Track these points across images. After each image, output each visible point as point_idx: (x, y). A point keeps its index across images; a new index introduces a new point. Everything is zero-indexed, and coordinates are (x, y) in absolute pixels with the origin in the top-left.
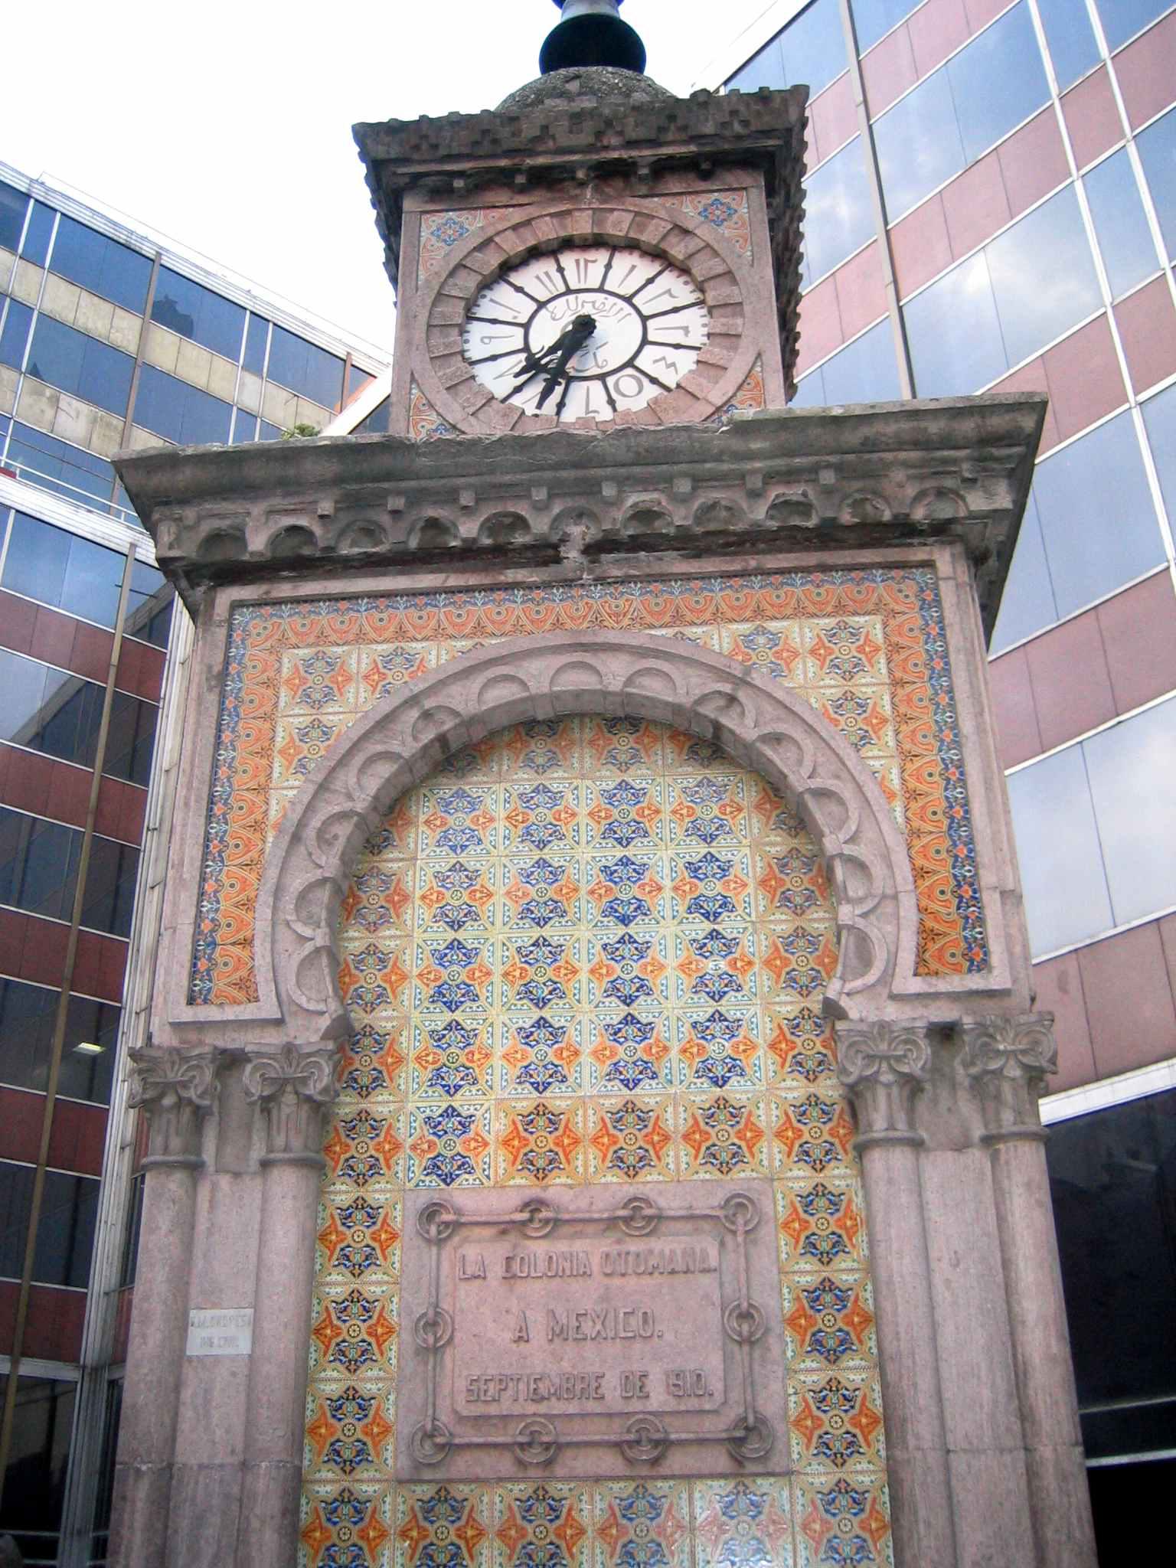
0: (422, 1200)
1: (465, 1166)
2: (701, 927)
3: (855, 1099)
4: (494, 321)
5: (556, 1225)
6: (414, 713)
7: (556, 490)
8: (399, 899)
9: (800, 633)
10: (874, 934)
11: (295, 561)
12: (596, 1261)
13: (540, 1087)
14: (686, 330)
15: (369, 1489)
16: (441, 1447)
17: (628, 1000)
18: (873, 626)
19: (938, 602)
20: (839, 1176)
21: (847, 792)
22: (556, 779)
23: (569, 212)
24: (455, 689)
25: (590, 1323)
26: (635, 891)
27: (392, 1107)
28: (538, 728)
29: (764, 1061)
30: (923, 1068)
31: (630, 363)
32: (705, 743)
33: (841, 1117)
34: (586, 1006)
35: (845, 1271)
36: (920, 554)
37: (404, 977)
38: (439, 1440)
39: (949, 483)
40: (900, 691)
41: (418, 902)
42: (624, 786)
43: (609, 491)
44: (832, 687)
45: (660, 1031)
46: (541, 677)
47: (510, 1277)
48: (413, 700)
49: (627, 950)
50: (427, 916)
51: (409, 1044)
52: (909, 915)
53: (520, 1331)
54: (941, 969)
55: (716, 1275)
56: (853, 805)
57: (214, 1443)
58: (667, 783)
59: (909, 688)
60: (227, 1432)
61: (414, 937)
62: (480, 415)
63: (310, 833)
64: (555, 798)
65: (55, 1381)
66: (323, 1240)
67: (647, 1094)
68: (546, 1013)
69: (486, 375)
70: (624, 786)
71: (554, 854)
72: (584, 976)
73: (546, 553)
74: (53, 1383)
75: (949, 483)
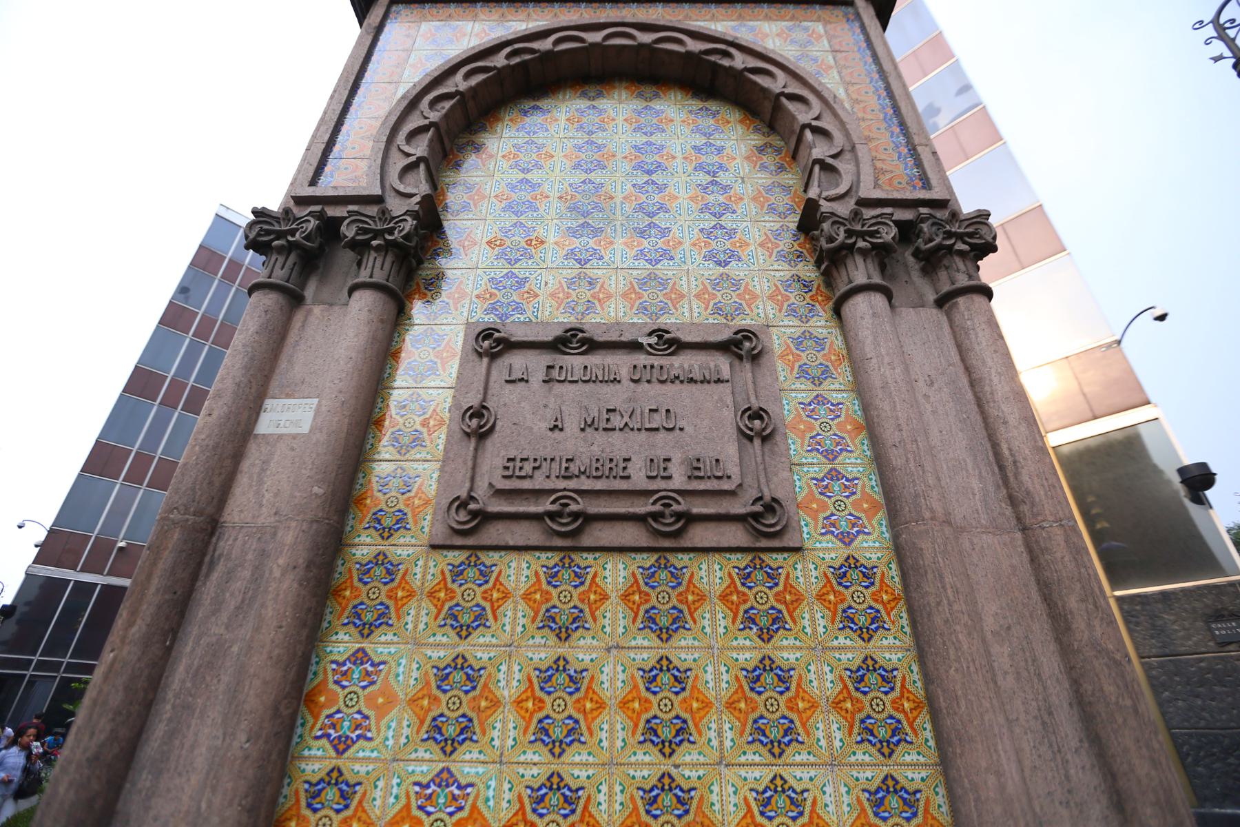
12: (624, 373)
15: (403, 552)
16: (474, 514)
25: (619, 418)
30: (893, 238)
33: (818, 288)
38: (472, 506)
53: (556, 420)
55: (729, 384)
57: (261, 506)
60: (276, 495)
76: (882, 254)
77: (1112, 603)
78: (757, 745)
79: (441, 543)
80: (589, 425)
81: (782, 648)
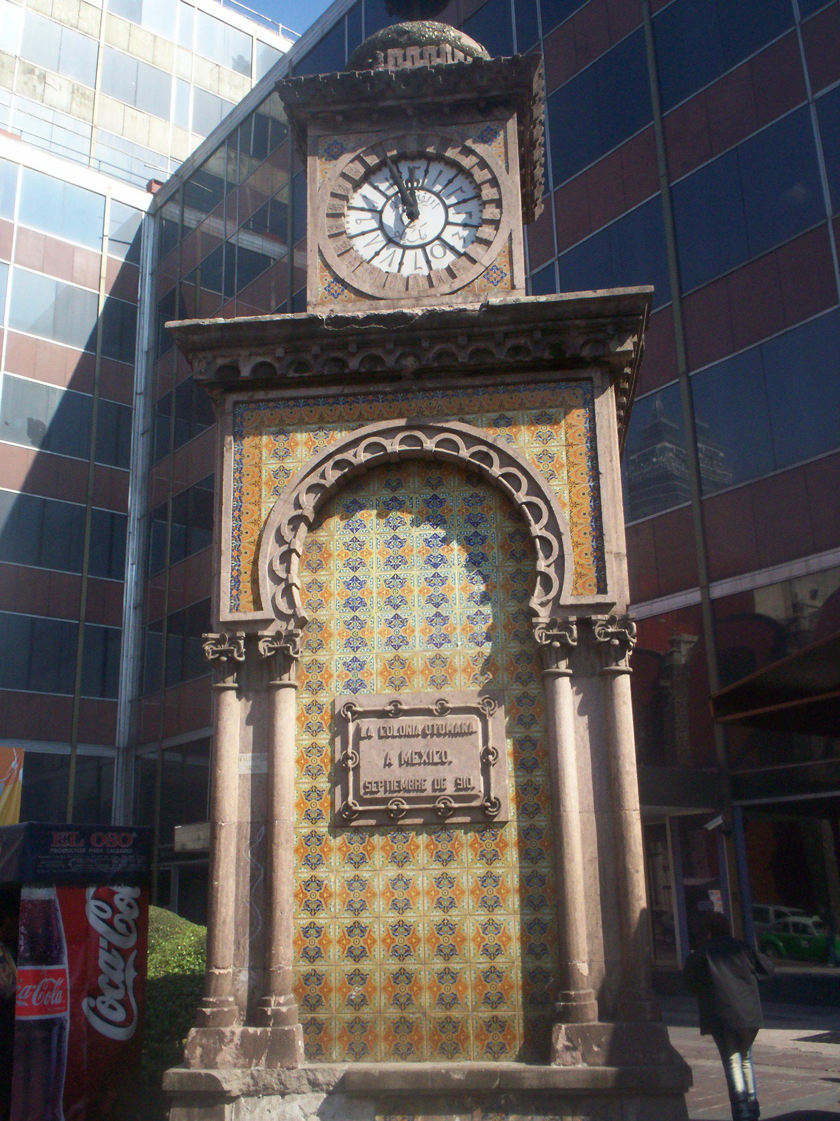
1: (362, 685)
13: (397, 647)
17: (437, 605)
23: (404, 137)
27: (328, 657)
31: (438, 238)
34: (416, 607)
36: (585, 374)
37: (331, 595)
39: (600, 336)
40: (571, 450)
41: (336, 558)
43: (425, 344)
45: (452, 621)
49: (436, 581)
50: (341, 564)
54: (584, 592)
59: (575, 448)
62: (357, 272)
65: (99, 757)
67: (446, 650)
68: (398, 612)
69: (359, 244)
70: (435, 497)
72: (416, 593)
73: (393, 376)
74: (99, 758)
75: (600, 336)
77: (549, 262)
78: (455, 972)
81: (496, 868)
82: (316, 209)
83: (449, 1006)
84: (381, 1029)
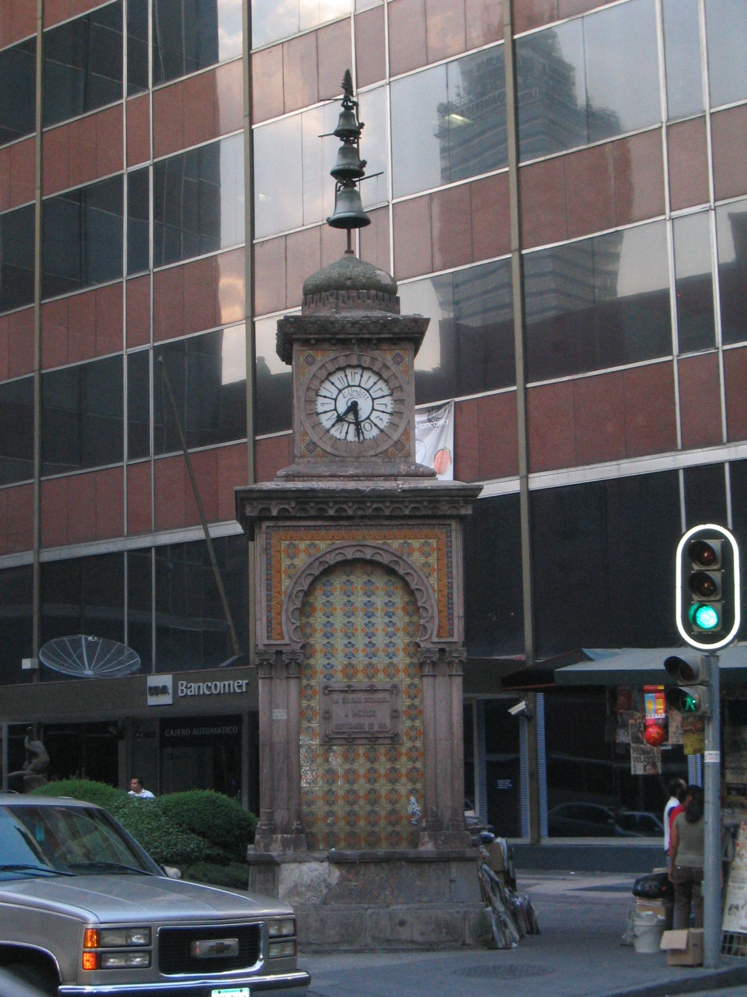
0: (323, 684)
2: (387, 620)
3: (422, 665)
4: (325, 397)
5: (354, 691)
6: (317, 563)
7: (354, 503)
8: (314, 610)
9: (416, 544)
10: (428, 627)
11: (283, 516)
12: (363, 700)
14: (386, 405)
18: (434, 542)
19: (451, 536)
20: (416, 681)
21: (424, 590)
22: (353, 578)
24: (328, 556)
26: (372, 609)
28: (347, 565)
29: (401, 654)
32: (389, 571)
35: (417, 702)
42: (369, 581)
44: (422, 560)
45: (377, 645)
46: (350, 554)
47: (344, 703)
48: (317, 559)
51: (318, 647)
52: (436, 622)
56: (425, 596)
58: (380, 581)
61: (318, 620)
63: (294, 596)
64: (352, 583)
66: (301, 694)
67: (374, 660)
69: (323, 418)
70: (369, 581)
71: (352, 599)
73: (350, 518)
76: (434, 664)
79: (526, 292)
80: (355, 715)
82: (299, 398)
83: (373, 826)
84: (342, 836)
